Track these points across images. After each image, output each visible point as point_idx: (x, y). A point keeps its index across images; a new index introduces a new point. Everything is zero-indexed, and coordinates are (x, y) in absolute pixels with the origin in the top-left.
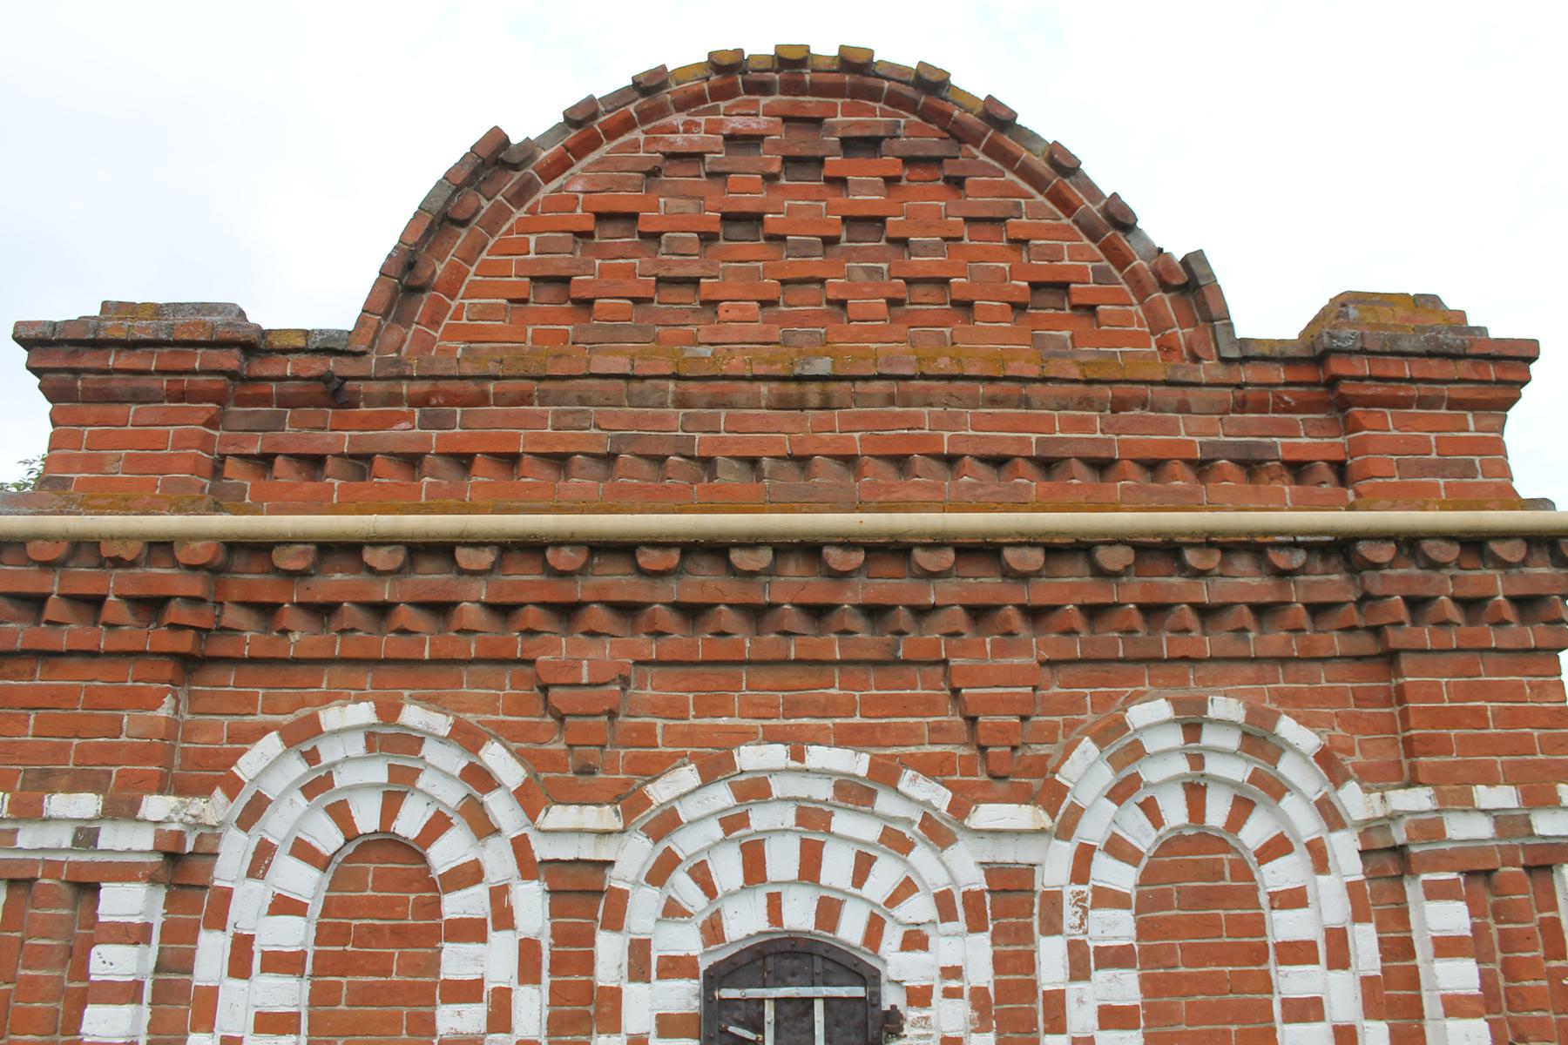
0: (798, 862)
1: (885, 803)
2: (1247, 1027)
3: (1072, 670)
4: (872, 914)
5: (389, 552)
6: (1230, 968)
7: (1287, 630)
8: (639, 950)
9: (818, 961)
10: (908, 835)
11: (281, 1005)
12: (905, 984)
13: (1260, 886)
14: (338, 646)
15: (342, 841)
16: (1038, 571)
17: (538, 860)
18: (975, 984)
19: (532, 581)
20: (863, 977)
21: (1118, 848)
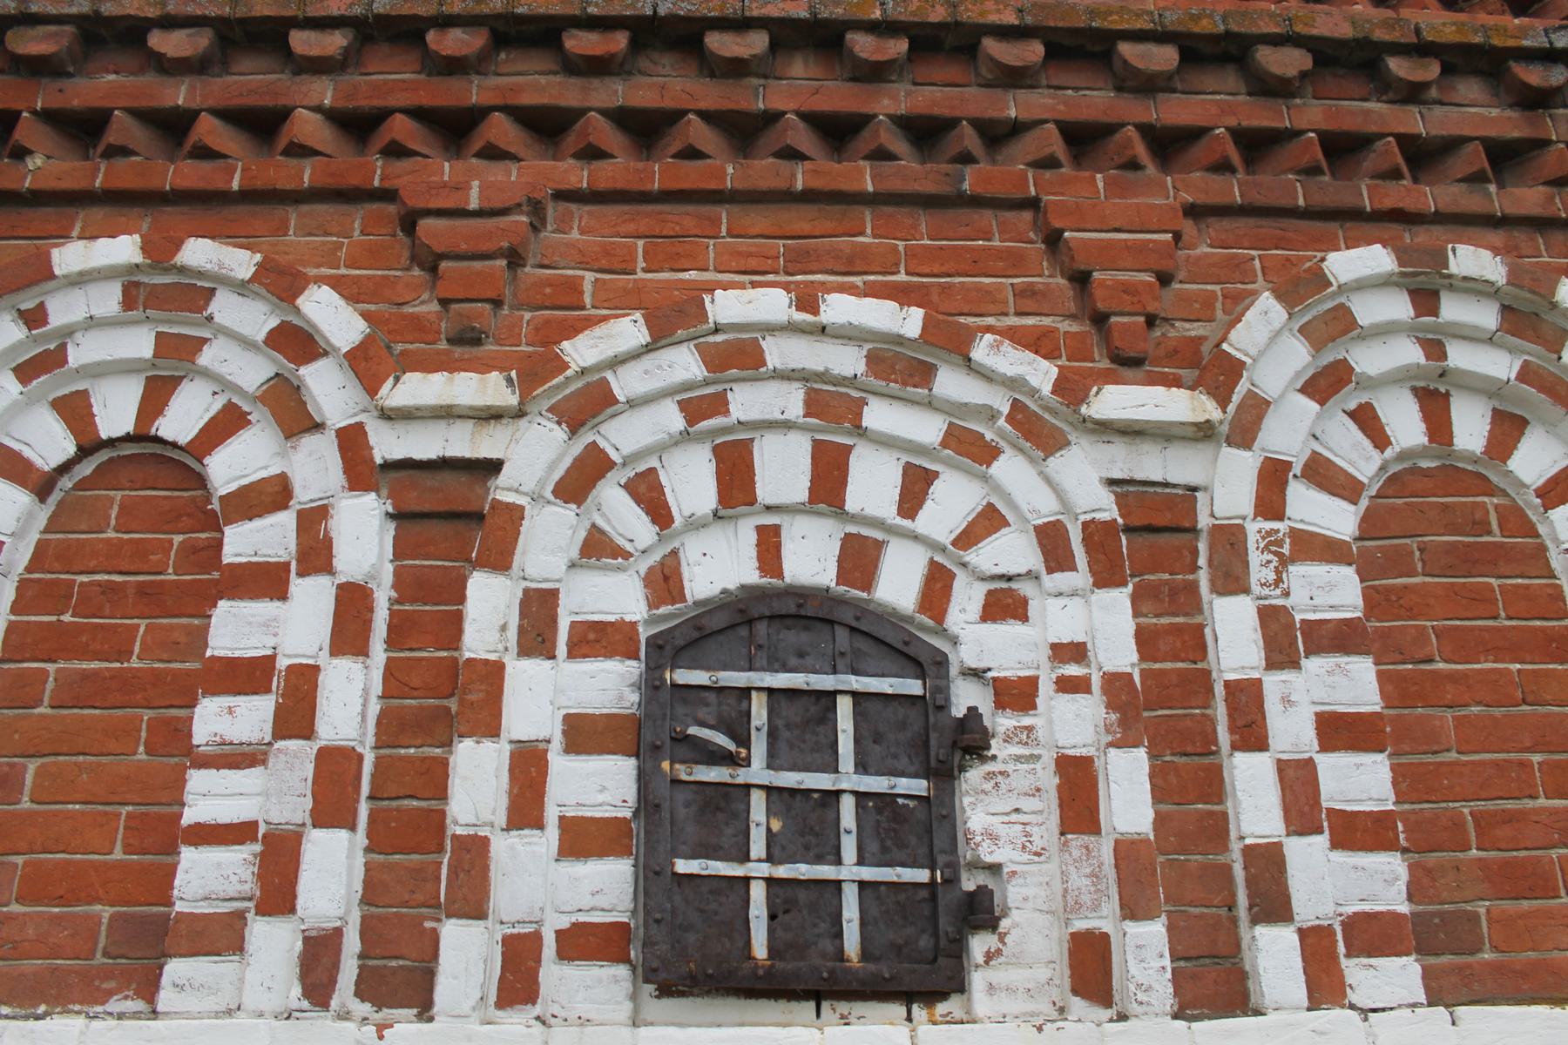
0: (809, 477)
1: (950, 383)
2: (1557, 757)
3: (1227, 224)
4: (933, 564)
5: (188, 36)
9: (842, 635)
10: (989, 436)
12: (990, 675)
13: (1549, 543)
14: (101, 176)
17: (379, 461)
18: (1109, 667)
19: (404, 81)
20: (919, 664)
21: (1322, 474)
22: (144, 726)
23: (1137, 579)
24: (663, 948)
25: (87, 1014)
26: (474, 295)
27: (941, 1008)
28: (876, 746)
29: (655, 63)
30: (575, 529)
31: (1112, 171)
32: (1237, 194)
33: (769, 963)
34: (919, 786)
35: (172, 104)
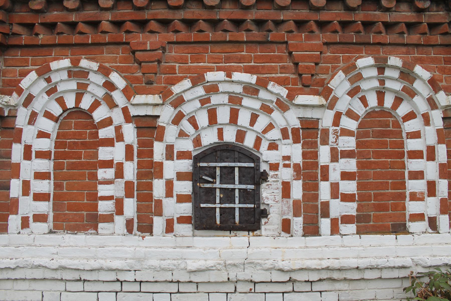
1: (263, 94)
3: (335, 47)
4: (257, 136)
6: (390, 160)
7: (419, 34)
8: (170, 149)
9: (236, 153)
11: (43, 170)
12: (269, 162)
13: (403, 130)
14: (57, 40)
15: (62, 111)
16: (324, 7)
17: (132, 116)
18: (295, 162)
19: (128, 12)
21: (350, 114)
22: (87, 174)
23: (304, 140)
24: (198, 223)
25: (85, 233)
26: (150, 72)
27: (255, 232)
28: (243, 178)
29: (191, 5)
30: (177, 131)
31: (306, 33)
32: (338, 39)
33: (220, 225)
34: (252, 187)
35: (72, 21)
